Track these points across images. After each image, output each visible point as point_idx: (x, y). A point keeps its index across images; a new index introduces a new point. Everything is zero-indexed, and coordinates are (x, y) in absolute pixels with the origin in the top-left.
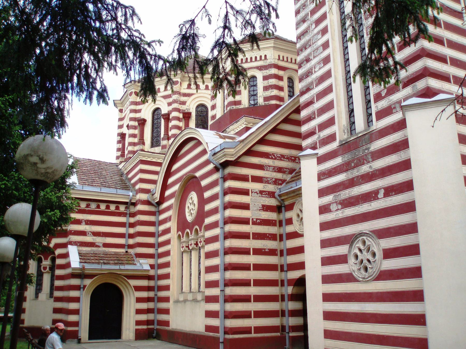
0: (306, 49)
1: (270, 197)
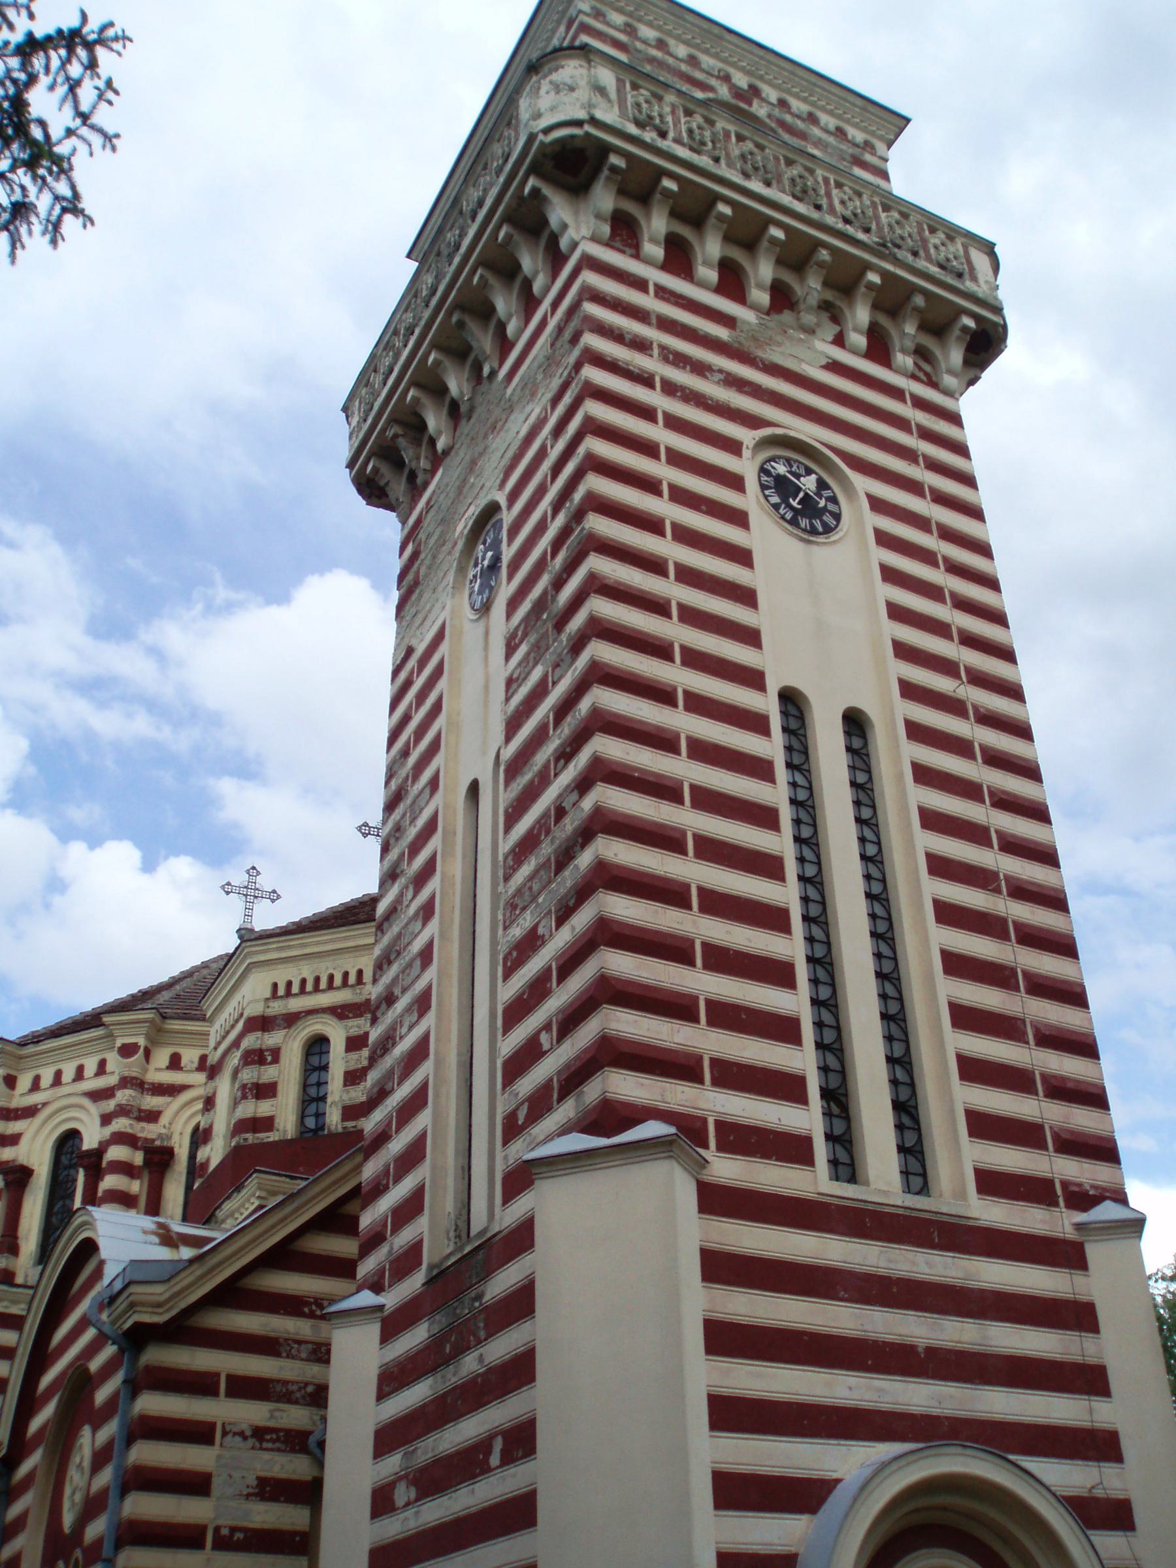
0: (390, 963)
1: (293, 1451)
